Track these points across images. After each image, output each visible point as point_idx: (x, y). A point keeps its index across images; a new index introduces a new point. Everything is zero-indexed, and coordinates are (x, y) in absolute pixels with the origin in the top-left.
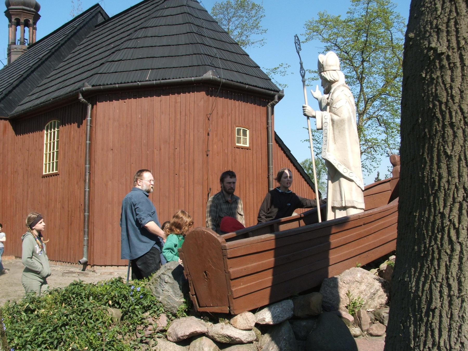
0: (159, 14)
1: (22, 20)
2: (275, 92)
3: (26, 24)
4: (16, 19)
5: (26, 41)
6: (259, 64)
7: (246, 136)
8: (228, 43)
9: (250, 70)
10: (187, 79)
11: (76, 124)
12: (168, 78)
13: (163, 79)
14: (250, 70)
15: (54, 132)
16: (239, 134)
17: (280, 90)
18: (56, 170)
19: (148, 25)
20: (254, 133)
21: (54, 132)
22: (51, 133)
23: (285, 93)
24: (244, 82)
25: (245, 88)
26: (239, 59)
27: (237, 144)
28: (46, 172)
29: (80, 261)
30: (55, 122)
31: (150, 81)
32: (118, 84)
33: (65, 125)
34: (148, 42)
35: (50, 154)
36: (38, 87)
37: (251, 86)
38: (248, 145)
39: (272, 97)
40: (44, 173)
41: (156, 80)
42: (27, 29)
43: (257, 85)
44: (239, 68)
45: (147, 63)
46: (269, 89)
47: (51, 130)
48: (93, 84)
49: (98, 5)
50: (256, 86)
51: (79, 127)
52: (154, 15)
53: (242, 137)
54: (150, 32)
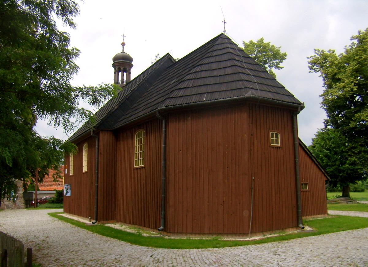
0: (209, 55)
1: (122, 69)
3: (125, 71)
4: (118, 68)
5: (124, 81)
8: (261, 72)
13: (216, 99)
15: (141, 139)
16: (273, 137)
17: (301, 103)
18: (143, 157)
19: (210, 55)
21: (141, 139)
22: (139, 140)
23: (305, 105)
26: (270, 83)
27: (272, 144)
28: (136, 165)
29: (159, 229)
30: (141, 132)
31: (206, 101)
32: (184, 104)
34: (203, 74)
35: (139, 146)
36: (131, 109)
37: (281, 101)
38: (279, 145)
40: (135, 167)
41: (211, 100)
42: (125, 74)
43: (285, 101)
45: (203, 90)
46: (293, 103)
47: (139, 137)
48: (166, 105)
49: (168, 54)
50: (284, 101)
52: (198, 64)
53: (275, 139)
54: (204, 68)
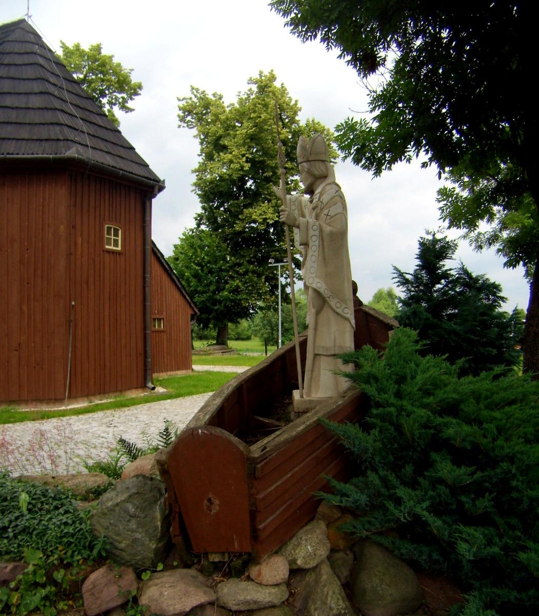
2: (154, 182)
6: (134, 144)
7: (118, 236)
9: (122, 152)
10: (32, 156)
11: (505, 260)
12: (17, 152)
14: (122, 152)
20: (127, 232)
24: (118, 167)
25: (119, 173)
27: (107, 247)
33: (182, 240)
38: (119, 248)
39: (153, 187)
43: (134, 172)
44: (109, 148)
46: (147, 178)
51: (505, 264)
